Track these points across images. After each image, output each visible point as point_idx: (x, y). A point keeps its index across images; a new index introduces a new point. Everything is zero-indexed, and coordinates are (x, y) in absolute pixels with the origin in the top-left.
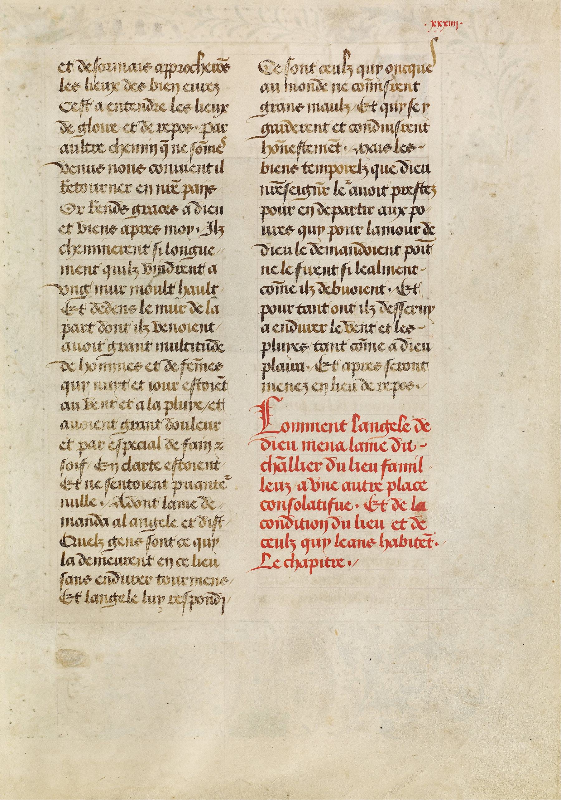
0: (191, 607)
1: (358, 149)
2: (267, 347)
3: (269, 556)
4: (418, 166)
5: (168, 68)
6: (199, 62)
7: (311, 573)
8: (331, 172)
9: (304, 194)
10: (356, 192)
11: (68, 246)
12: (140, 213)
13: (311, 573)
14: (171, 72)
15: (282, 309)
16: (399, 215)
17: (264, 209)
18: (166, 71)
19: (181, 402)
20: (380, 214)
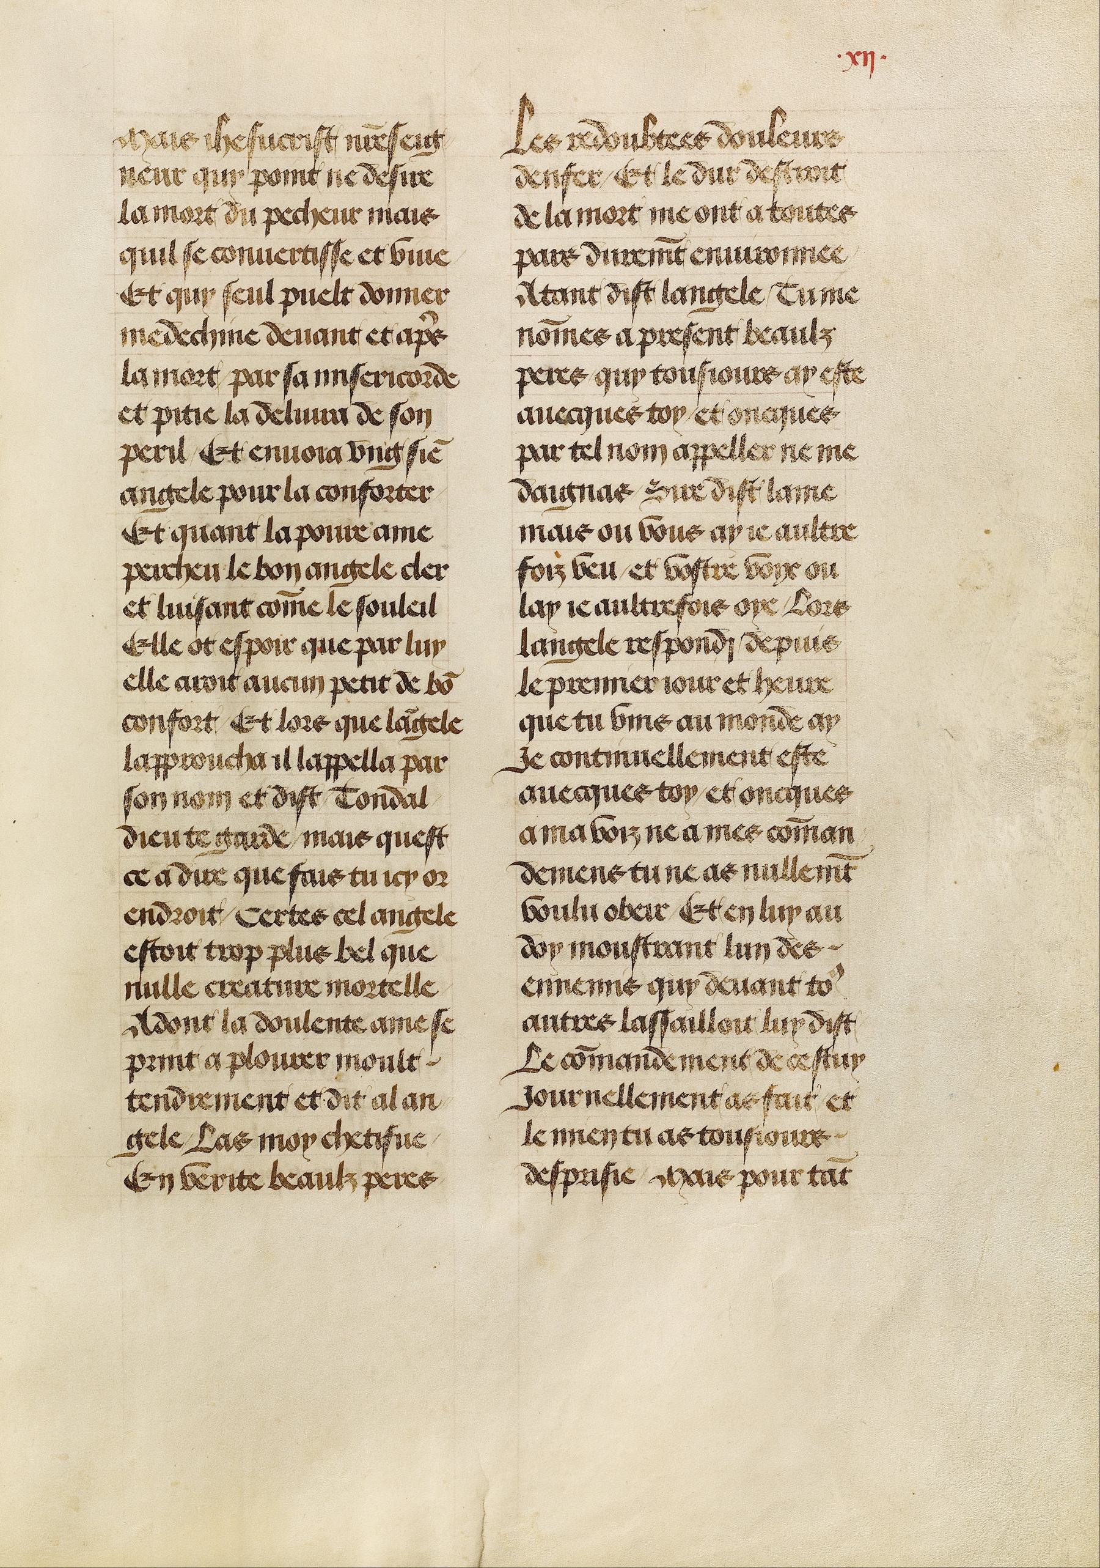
1: (666, 1177)
3: (538, 1050)
4: (258, 448)
9: (388, 459)
10: (532, 797)
15: (257, 494)
16: (187, 580)
17: (224, 491)
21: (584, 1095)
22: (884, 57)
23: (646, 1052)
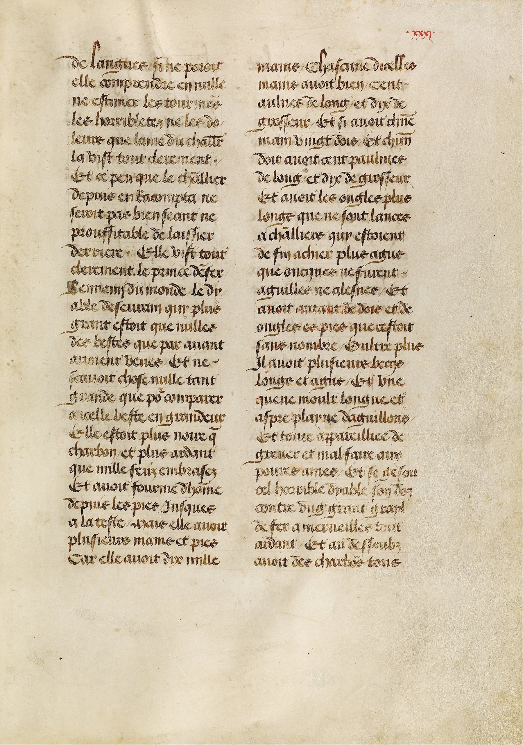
0: (186, 75)
2: (145, 436)
5: (329, 437)
6: (309, 249)
7: (309, 247)
8: (191, 402)
9: (380, 257)
11: (393, 120)
12: (173, 420)
13: (309, 247)
14: (332, 440)
16: (193, 494)
18: (327, 439)
19: (84, 538)
20: (330, 548)
21: (160, 488)
22: (434, 33)
23: (152, 80)
